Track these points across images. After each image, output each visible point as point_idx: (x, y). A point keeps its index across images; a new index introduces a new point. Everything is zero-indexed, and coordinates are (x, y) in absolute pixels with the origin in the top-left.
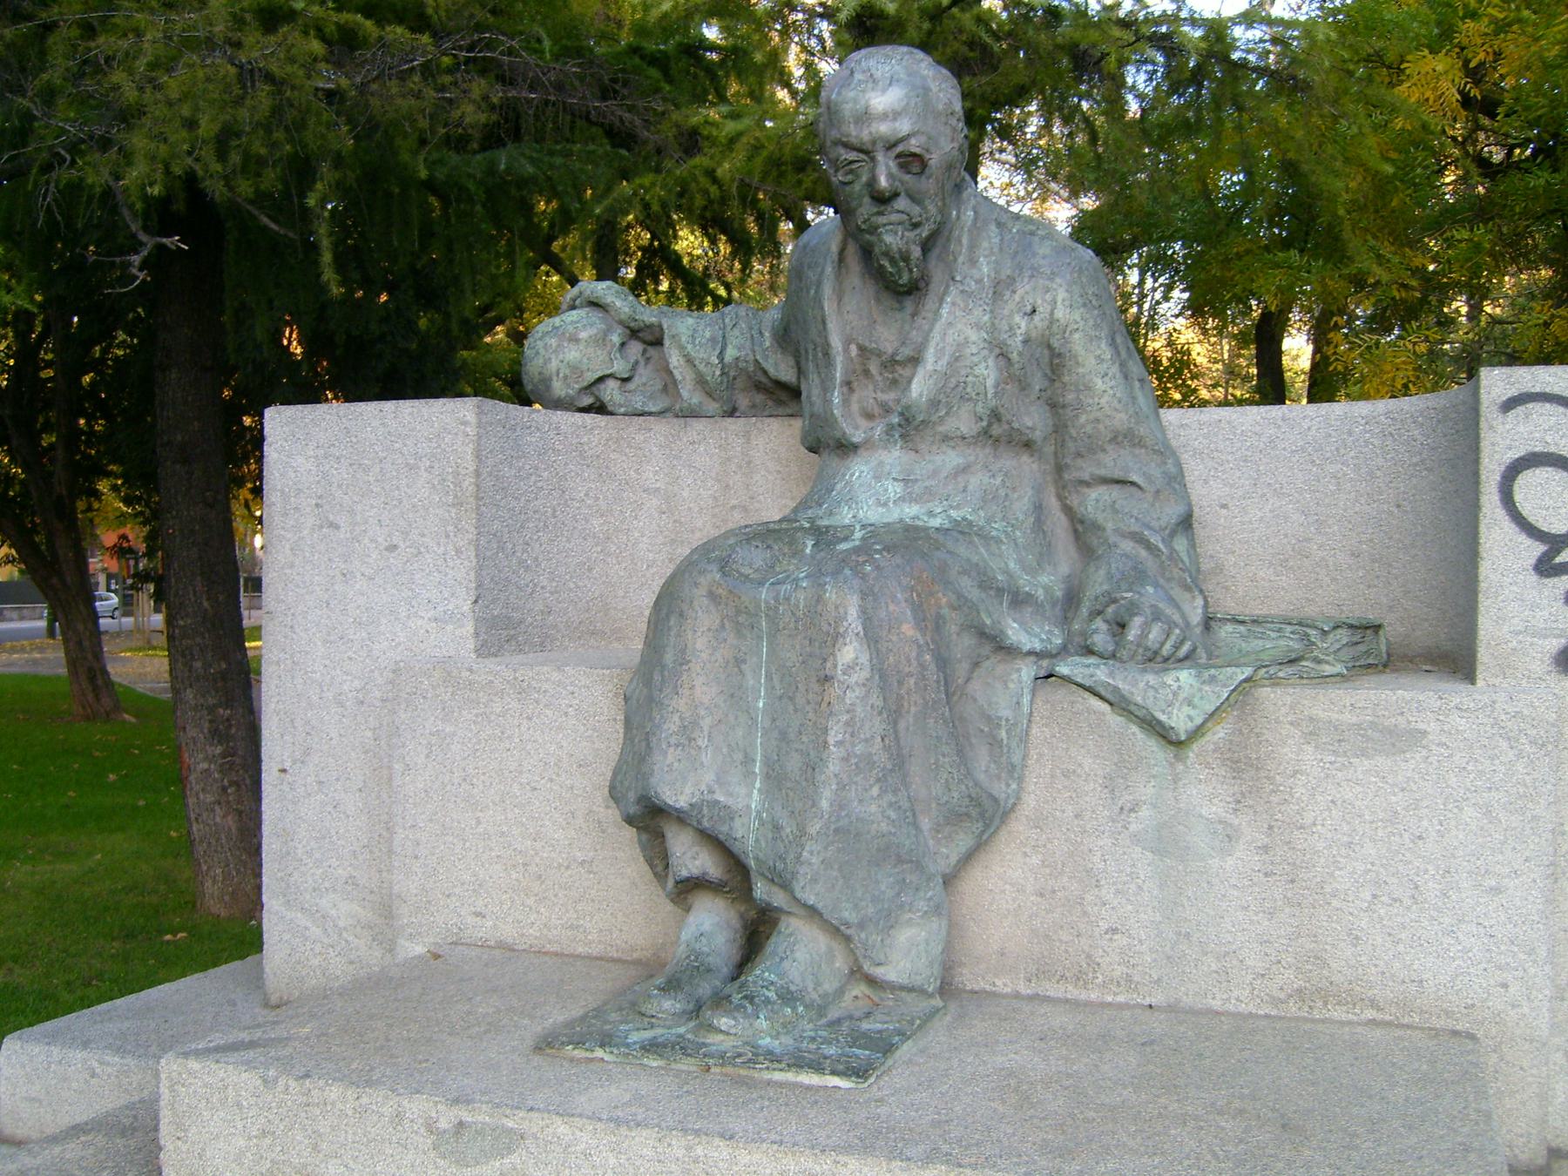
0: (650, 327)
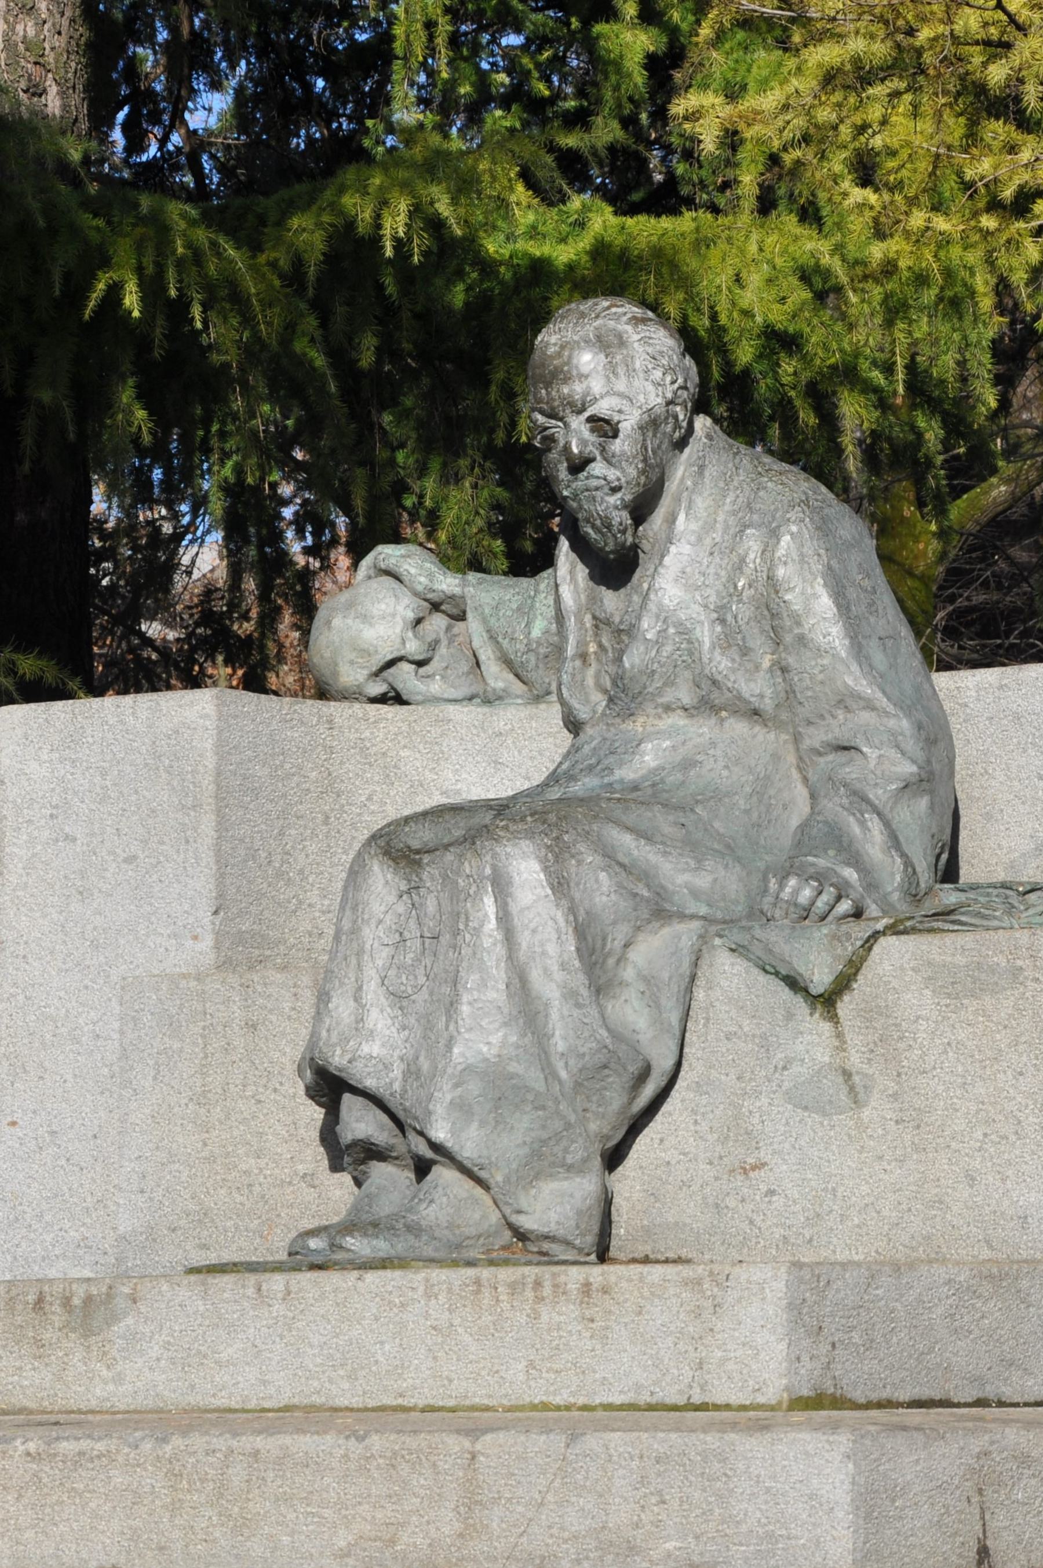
0: (452, 597)
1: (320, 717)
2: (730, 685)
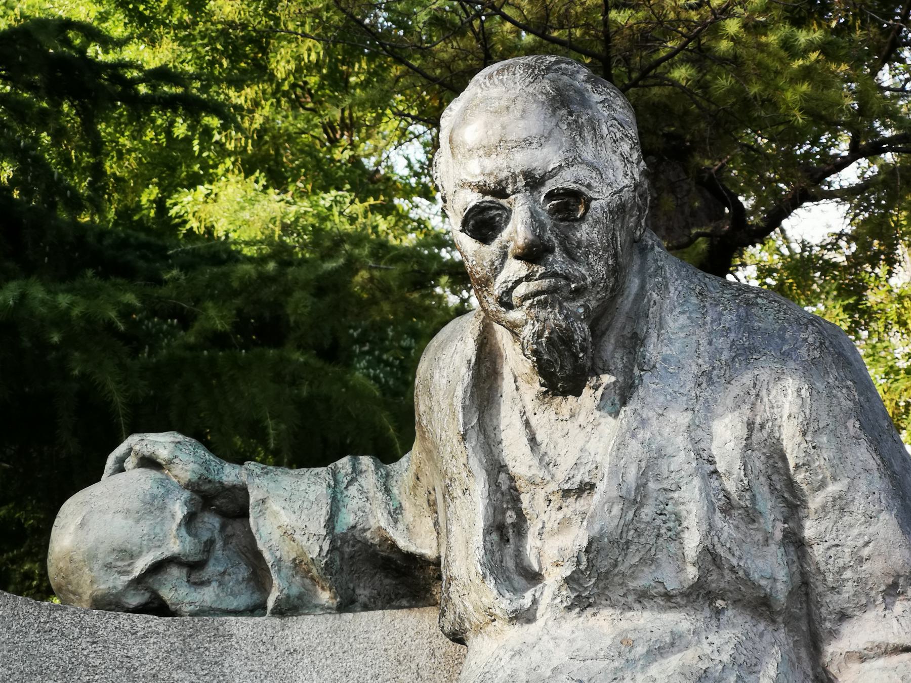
1: (82, 628)
2: (734, 562)
